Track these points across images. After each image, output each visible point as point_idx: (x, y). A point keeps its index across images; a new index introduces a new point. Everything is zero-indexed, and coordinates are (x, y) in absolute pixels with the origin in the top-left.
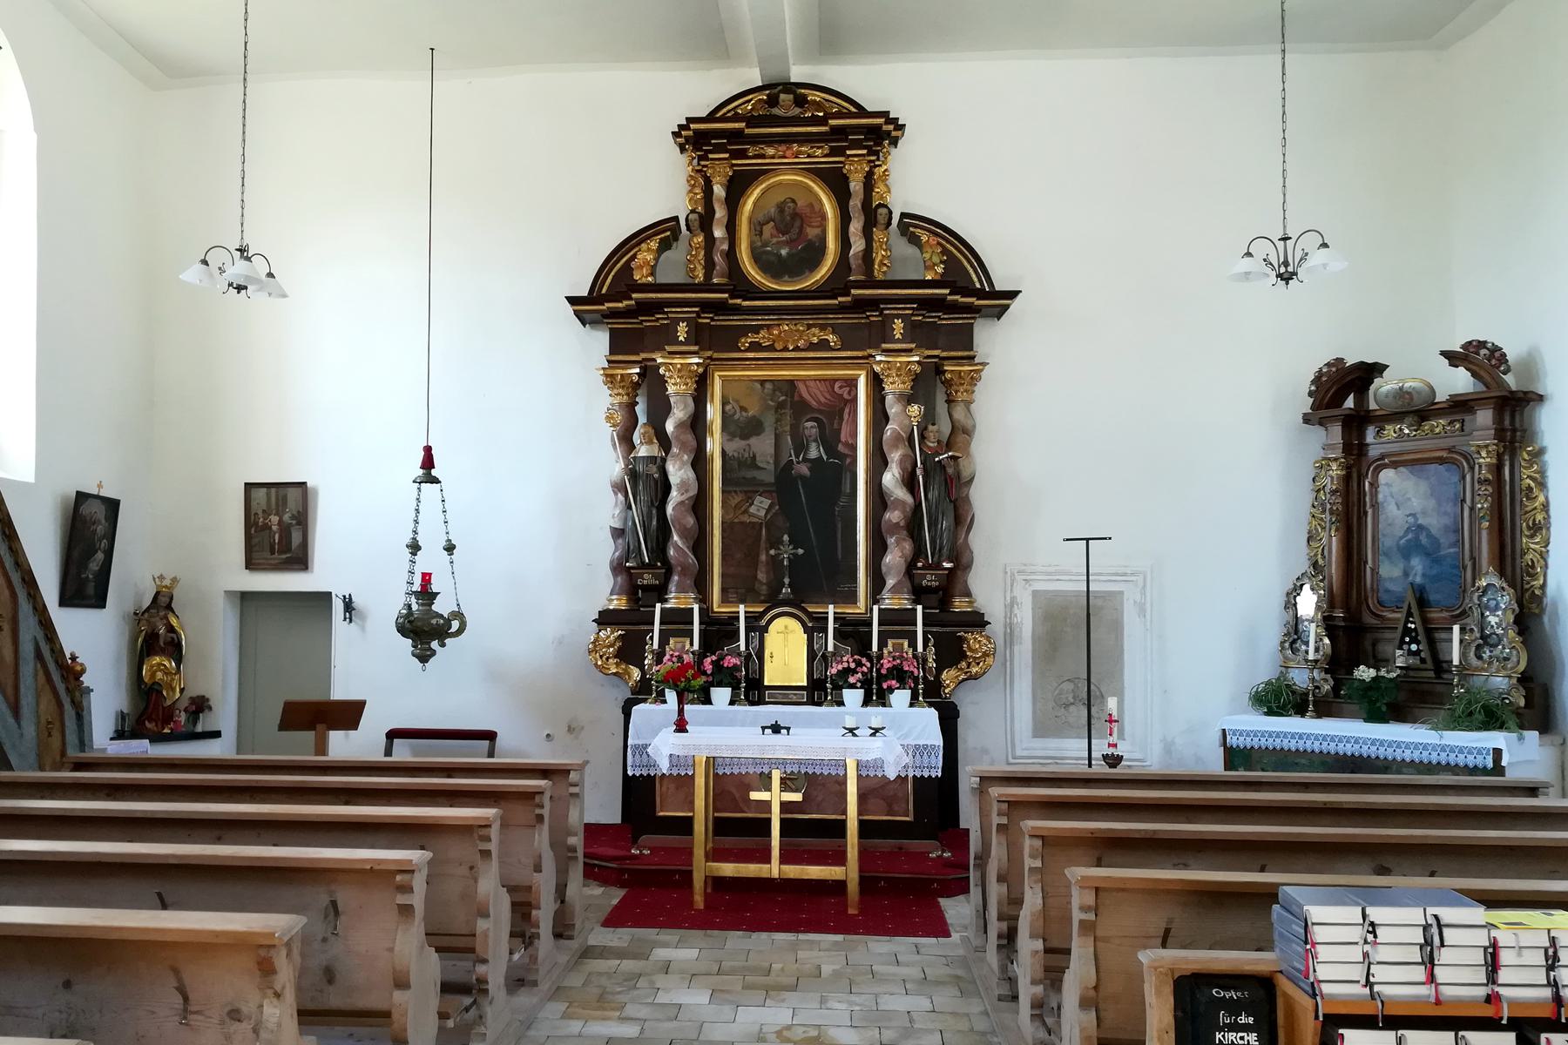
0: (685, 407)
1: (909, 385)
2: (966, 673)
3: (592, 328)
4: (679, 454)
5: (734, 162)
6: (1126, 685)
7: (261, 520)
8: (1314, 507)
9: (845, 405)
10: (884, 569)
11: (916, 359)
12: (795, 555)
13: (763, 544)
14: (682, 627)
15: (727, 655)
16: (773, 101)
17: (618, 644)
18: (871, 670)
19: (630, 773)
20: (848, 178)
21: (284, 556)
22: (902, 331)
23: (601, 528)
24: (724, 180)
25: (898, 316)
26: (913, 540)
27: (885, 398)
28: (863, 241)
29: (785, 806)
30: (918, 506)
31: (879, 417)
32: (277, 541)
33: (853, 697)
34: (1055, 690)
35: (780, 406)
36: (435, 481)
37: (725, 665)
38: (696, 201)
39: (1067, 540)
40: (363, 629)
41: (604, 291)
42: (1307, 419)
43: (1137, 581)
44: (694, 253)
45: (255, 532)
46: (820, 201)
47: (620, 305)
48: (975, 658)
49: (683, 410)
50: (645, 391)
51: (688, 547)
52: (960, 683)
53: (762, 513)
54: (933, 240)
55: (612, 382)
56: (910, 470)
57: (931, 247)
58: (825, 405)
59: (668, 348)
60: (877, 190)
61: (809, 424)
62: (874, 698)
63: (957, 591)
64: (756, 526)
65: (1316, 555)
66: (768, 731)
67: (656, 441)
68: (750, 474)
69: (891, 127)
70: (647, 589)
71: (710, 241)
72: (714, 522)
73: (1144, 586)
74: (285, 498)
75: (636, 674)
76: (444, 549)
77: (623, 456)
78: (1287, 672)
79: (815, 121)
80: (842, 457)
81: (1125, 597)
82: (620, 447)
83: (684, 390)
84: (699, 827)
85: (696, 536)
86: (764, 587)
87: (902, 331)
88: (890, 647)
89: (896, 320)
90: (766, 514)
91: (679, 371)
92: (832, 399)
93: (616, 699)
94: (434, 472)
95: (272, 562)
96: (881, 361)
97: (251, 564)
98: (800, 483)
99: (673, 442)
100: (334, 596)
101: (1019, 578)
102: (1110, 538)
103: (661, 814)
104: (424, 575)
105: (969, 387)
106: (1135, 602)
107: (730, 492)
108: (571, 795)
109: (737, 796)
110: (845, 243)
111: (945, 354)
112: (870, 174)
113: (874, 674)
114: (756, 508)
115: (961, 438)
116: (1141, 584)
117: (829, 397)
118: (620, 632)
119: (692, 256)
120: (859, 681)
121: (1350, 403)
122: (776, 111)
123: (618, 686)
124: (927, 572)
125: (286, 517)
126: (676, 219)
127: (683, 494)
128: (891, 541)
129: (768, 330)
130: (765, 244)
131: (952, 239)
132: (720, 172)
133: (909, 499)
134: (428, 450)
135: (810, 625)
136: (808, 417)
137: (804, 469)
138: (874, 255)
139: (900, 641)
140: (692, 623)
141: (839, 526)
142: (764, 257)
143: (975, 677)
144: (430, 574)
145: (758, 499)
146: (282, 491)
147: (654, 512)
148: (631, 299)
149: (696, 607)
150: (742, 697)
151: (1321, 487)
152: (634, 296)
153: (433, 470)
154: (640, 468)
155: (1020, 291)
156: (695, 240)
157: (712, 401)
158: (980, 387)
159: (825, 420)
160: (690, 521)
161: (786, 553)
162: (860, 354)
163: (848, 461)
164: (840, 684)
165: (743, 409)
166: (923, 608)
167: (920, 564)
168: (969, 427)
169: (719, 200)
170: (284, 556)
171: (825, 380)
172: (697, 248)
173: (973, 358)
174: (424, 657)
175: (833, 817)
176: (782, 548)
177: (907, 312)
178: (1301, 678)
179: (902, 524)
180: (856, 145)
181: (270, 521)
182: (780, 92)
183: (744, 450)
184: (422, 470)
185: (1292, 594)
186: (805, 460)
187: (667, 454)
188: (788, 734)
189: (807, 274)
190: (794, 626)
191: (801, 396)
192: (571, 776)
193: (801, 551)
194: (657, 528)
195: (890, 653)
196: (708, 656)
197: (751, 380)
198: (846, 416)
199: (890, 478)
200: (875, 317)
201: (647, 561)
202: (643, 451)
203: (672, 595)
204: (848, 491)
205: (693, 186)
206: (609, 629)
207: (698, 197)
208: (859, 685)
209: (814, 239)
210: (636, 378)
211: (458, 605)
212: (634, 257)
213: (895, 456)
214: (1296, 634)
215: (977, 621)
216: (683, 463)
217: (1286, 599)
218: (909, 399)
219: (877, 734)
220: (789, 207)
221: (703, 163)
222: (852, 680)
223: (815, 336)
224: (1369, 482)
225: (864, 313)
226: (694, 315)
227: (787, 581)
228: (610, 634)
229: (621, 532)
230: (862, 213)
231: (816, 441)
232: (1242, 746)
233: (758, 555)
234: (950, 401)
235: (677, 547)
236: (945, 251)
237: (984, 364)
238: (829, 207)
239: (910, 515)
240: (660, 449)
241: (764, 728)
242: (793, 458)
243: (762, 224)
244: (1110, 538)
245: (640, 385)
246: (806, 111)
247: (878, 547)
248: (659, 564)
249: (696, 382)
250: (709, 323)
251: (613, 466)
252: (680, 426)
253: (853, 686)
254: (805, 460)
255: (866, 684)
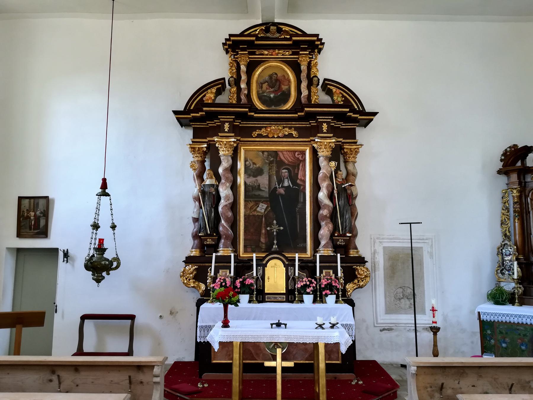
0: (228, 161)
1: (330, 153)
2: (357, 285)
3: (185, 128)
4: (225, 183)
5: (250, 56)
6: (425, 289)
7: (26, 214)
8: (503, 209)
9: (300, 163)
10: (320, 236)
11: (334, 141)
12: (279, 230)
13: (263, 225)
14: (225, 264)
15: (247, 278)
16: (267, 30)
17: (195, 273)
18: (316, 285)
19: (198, 340)
20: (300, 64)
21: (36, 231)
22: (327, 129)
23: (188, 218)
24: (246, 63)
25: (325, 122)
26: (332, 223)
27: (319, 159)
28: (307, 91)
29: (284, 369)
30: (335, 208)
31: (316, 168)
32: (33, 224)
33: (308, 298)
34: (395, 292)
35: (271, 163)
36: (107, 195)
37: (246, 283)
38: (233, 73)
39: (401, 223)
40: (73, 266)
41: (192, 108)
42: (499, 172)
43: (428, 242)
44: (232, 95)
45: (22, 219)
46: (288, 74)
47: (198, 115)
48: (361, 278)
49: (227, 162)
50: (209, 156)
51: (229, 226)
52: (354, 290)
53: (263, 211)
54: (338, 91)
55: (194, 151)
56: (331, 191)
57: (337, 94)
58: (291, 162)
59: (220, 134)
60: (313, 70)
61: (284, 171)
62: (318, 299)
63: (351, 247)
64: (260, 217)
65: (506, 230)
66: (274, 326)
67: (214, 177)
68: (257, 193)
69: (319, 43)
70: (209, 246)
71: (239, 89)
72: (241, 215)
73: (432, 245)
74: (38, 204)
75: (203, 287)
76: (111, 227)
77: (198, 184)
78: (500, 284)
79: (285, 39)
80: (299, 185)
81: (424, 249)
82: (197, 181)
83: (227, 153)
84: (236, 369)
85: (232, 222)
86: (264, 245)
87: (327, 129)
88: (324, 274)
89: (324, 124)
90: (265, 211)
91: (225, 145)
92: (294, 160)
93: (194, 298)
94: (107, 191)
95: (29, 234)
96: (318, 142)
97: (19, 235)
98: (280, 197)
99: (222, 177)
100: (59, 250)
101: (377, 241)
102: (421, 223)
103: (214, 362)
104: (100, 240)
105: (355, 156)
106: (428, 252)
107: (248, 201)
108: (155, 383)
109: (253, 351)
110: (299, 92)
111: (343, 141)
112: (309, 63)
113: (318, 287)
114: (260, 208)
115: (351, 178)
116: (430, 244)
117: (293, 159)
118: (196, 267)
119: (231, 96)
120: (311, 291)
121: (519, 164)
122: (268, 35)
123: (194, 292)
124: (340, 238)
125: (38, 213)
126: (224, 79)
127: (226, 201)
128: (323, 223)
129: (265, 128)
130: (263, 93)
131: (347, 91)
132: (243, 59)
133: (331, 204)
134: (104, 180)
135: (287, 263)
136: (284, 167)
137: (282, 191)
138: (312, 98)
139: (329, 271)
140: (230, 263)
141: (298, 217)
142: (263, 98)
143: (361, 287)
144: (103, 240)
145: (261, 205)
146: (36, 200)
147: (213, 210)
148: (202, 111)
149: (232, 255)
150: (255, 299)
151: (507, 201)
152: (204, 109)
153: (106, 190)
154: (207, 189)
155: (378, 113)
156: (233, 90)
157: (240, 160)
158: (358, 156)
159: (291, 169)
160: (230, 214)
161: (275, 229)
162: (307, 140)
163: (302, 187)
164: (302, 292)
165: (254, 163)
166: (340, 255)
167: (336, 235)
168: (355, 173)
169: (243, 72)
170: (36, 231)
171: (291, 151)
172: (233, 93)
173: (356, 143)
174: (98, 280)
175: (302, 362)
176: (273, 226)
177: (329, 120)
178: (509, 286)
179: (328, 215)
180: (304, 49)
181: (30, 215)
182: (271, 25)
183: (255, 182)
184: (101, 190)
185: (500, 248)
186: (282, 187)
187: (219, 183)
188: (286, 328)
189: (282, 105)
190: (279, 263)
191: (280, 158)
192: (154, 370)
193: (282, 228)
194: (214, 217)
195: (324, 276)
196: (238, 279)
197: (258, 151)
198: (301, 167)
199: (322, 195)
200: (313, 123)
201: (209, 233)
202: (208, 182)
203: (221, 249)
204: (302, 201)
205: (232, 67)
206: (190, 265)
207: (234, 71)
208: (311, 293)
209: (285, 90)
210: (205, 149)
211: (117, 254)
212: (205, 96)
213: (324, 185)
214: (503, 266)
215: (361, 261)
216: (227, 187)
217: (498, 251)
218: (330, 159)
219: (335, 327)
220: (274, 77)
221: (236, 57)
222: (308, 290)
223: (287, 131)
224: (530, 199)
225: (308, 121)
226: (232, 120)
227: (275, 242)
228: (191, 268)
229: (197, 219)
230: (307, 79)
231: (287, 178)
232: (489, 320)
233: (261, 230)
234: (346, 162)
235: (223, 226)
236: (343, 96)
237: (362, 145)
238: (291, 76)
239: (332, 211)
240: (215, 181)
241: (272, 324)
242: (277, 186)
243: (262, 84)
244: (421, 223)
245: (207, 153)
246: (281, 35)
247: (317, 227)
248: (215, 234)
249: (233, 150)
250: (239, 125)
251: (194, 189)
252: (225, 170)
253: (308, 293)
254: (282, 187)
255: (314, 292)
